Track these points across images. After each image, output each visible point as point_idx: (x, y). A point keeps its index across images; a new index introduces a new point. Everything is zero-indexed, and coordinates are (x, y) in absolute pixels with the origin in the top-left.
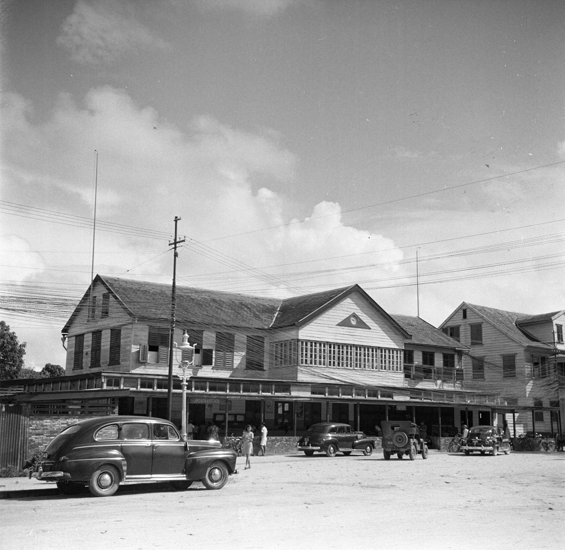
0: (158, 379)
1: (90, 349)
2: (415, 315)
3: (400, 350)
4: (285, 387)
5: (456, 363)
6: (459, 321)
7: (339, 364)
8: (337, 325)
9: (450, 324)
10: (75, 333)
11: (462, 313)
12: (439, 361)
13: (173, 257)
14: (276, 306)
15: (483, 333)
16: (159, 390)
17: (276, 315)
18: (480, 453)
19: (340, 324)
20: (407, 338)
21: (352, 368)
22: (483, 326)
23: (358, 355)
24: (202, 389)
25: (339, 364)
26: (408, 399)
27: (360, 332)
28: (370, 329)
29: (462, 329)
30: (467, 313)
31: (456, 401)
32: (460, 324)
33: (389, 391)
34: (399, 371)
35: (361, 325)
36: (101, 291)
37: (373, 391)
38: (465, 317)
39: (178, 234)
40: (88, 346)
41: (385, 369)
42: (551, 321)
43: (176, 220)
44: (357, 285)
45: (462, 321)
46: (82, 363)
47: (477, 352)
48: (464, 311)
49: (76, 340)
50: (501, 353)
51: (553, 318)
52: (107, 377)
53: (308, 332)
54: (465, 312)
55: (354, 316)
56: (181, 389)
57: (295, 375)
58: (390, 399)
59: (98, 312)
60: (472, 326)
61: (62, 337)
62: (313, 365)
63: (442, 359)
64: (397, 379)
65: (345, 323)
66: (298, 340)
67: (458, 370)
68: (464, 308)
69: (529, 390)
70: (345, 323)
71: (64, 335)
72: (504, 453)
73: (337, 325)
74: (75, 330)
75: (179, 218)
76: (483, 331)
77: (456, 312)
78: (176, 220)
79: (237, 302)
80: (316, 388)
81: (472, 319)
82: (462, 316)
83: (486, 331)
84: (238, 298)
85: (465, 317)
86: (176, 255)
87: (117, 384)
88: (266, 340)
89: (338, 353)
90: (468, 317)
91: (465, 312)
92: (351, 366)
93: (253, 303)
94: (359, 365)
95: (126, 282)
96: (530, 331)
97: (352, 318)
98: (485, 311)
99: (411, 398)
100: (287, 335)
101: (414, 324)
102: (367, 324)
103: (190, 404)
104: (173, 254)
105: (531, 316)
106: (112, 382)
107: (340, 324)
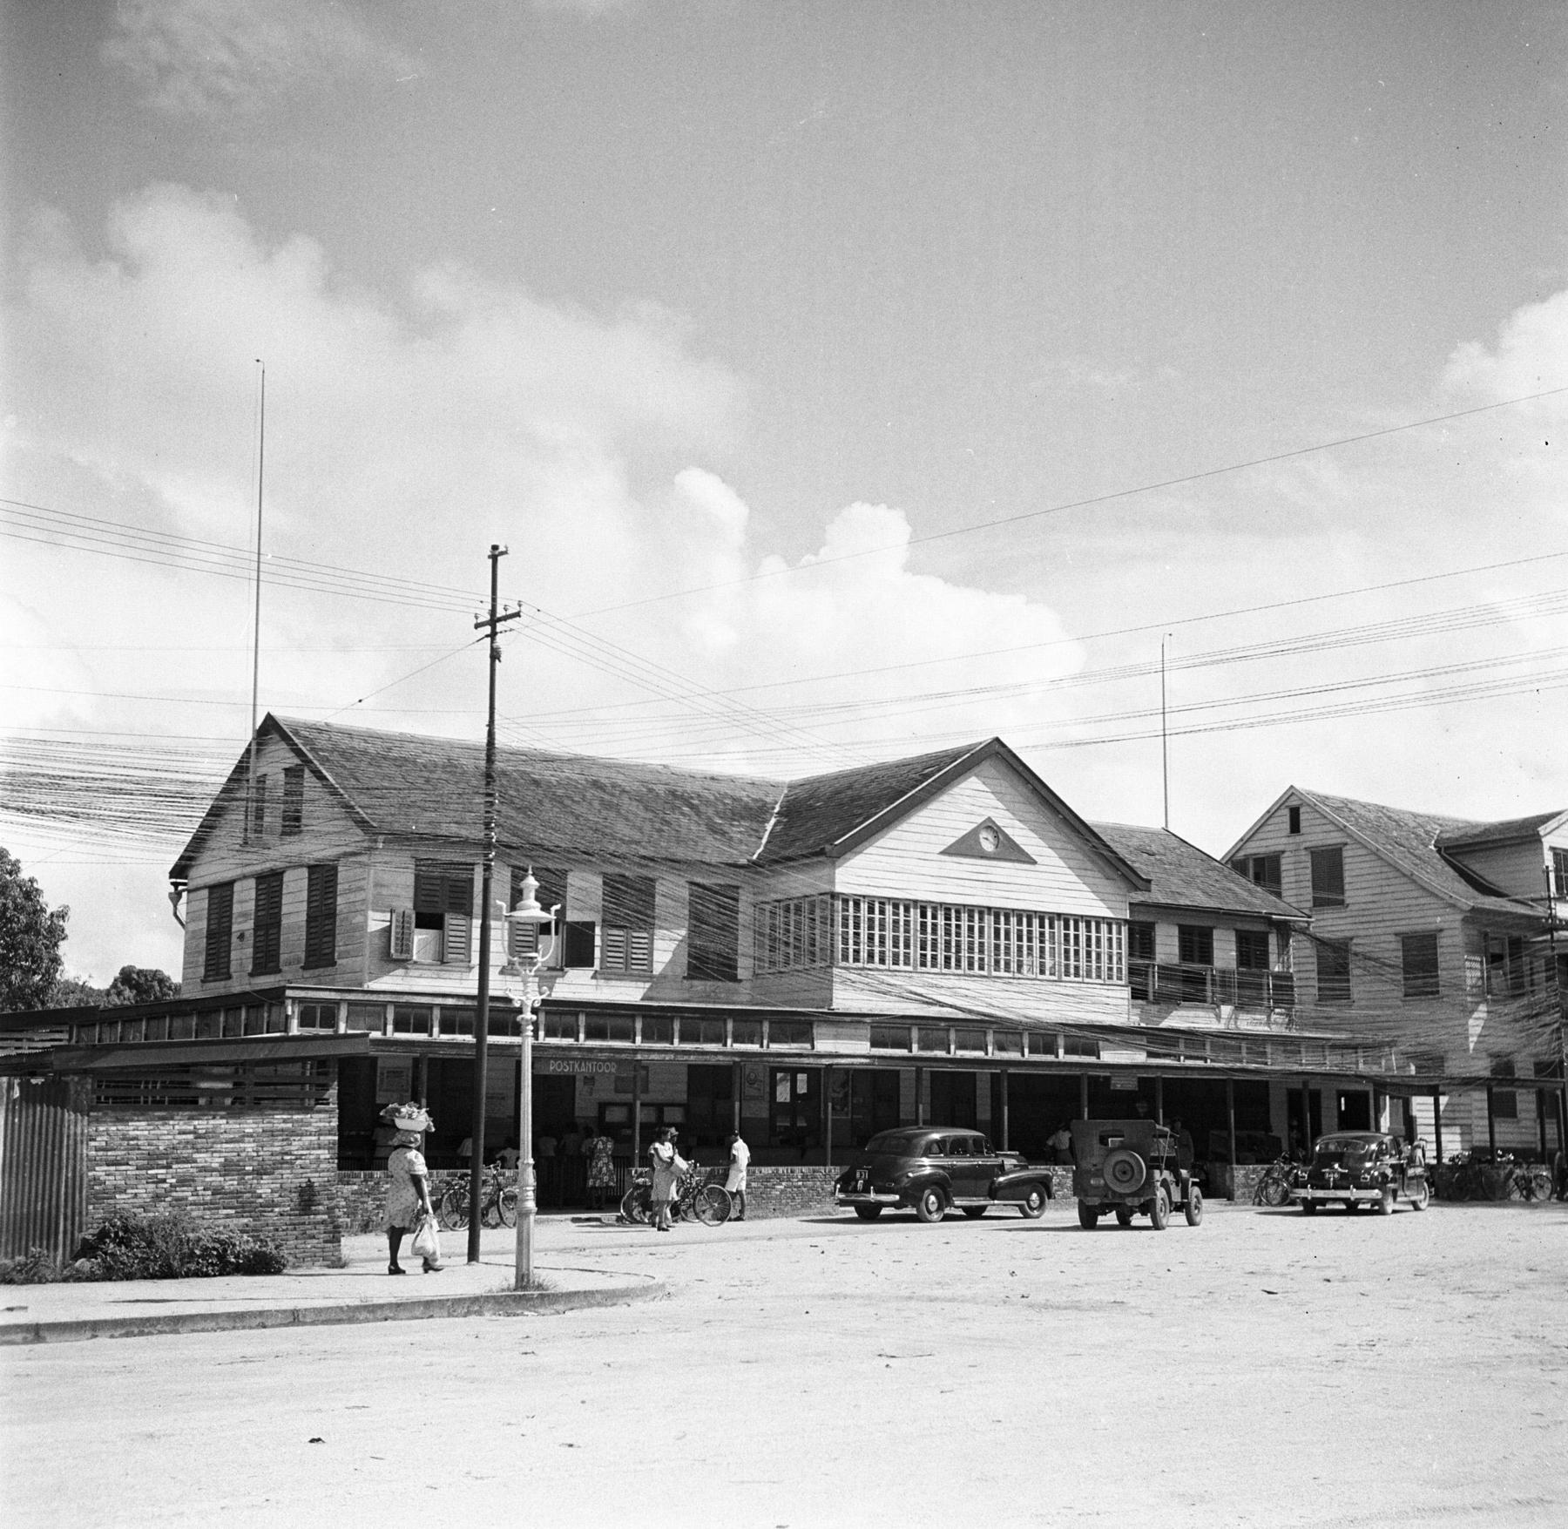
1: (250, 924)
2: (1157, 824)
3: (1119, 922)
4: (798, 1026)
5: (1273, 958)
6: (1277, 839)
9: (1256, 848)
11: (1287, 819)
12: (1225, 953)
14: (768, 800)
15: (1346, 874)
16: (445, 1037)
19: (953, 851)
20: (1137, 888)
21: (984, 973)
24: (565, 1035)
27: (1005, 870)
28: (1035, 863)
29: (1286, 864)
30: (1302, 817)
31: (1276, 1063)
33: (1088, 1036)
35: (1010, 851)
36: (276, 761)
38: (1295, 828)
40: (244, 915)
42: (1537, 840)
43: (495, 554)
44: (997, 739)
45: (1284, 840)
46: (229, 962)
47: (1330, 924)
50: (1399, 929)
51: (1542, 830)
52: (301, 1000)
53: (865, 872)
54: (1295, 813)
55: (990, 826)
57: (825, 993)
58: (1092, 1059)
59: (272, 819)
61: (172, 889)
62: (976, 971)
64: (1109, 1003)
65: (965, 848)
66: (834, 896)
67: (1277, 976)
68: (1294, 802)
69: (1475, 1031)
70: (965, 848)
71: (176, 885)
74: (209, 871)
75: (502, 549)
76: (1346, 867)
77: (1270, 815)
78: (495, 554)
79: (660, 789)
80: (886, 1029)
81: (1315, 834)
82: (1287, 826)
83: (1354, 867)
85: (1295, 828)
87: (330, 1019)
88: (745, 899)
89: (947, 931)
90: (1303, 830)
91: (1295, 813)
93: (706, 793)
94: (1004, 964)
96: (1476, 866)
97: (983, 834)
98: (1351, 810)
99: (873, 1045)
100: (798, 883)
102: (1026, 849)
104: (488, 652)
105: (1477, 826)
107: (953, 851)
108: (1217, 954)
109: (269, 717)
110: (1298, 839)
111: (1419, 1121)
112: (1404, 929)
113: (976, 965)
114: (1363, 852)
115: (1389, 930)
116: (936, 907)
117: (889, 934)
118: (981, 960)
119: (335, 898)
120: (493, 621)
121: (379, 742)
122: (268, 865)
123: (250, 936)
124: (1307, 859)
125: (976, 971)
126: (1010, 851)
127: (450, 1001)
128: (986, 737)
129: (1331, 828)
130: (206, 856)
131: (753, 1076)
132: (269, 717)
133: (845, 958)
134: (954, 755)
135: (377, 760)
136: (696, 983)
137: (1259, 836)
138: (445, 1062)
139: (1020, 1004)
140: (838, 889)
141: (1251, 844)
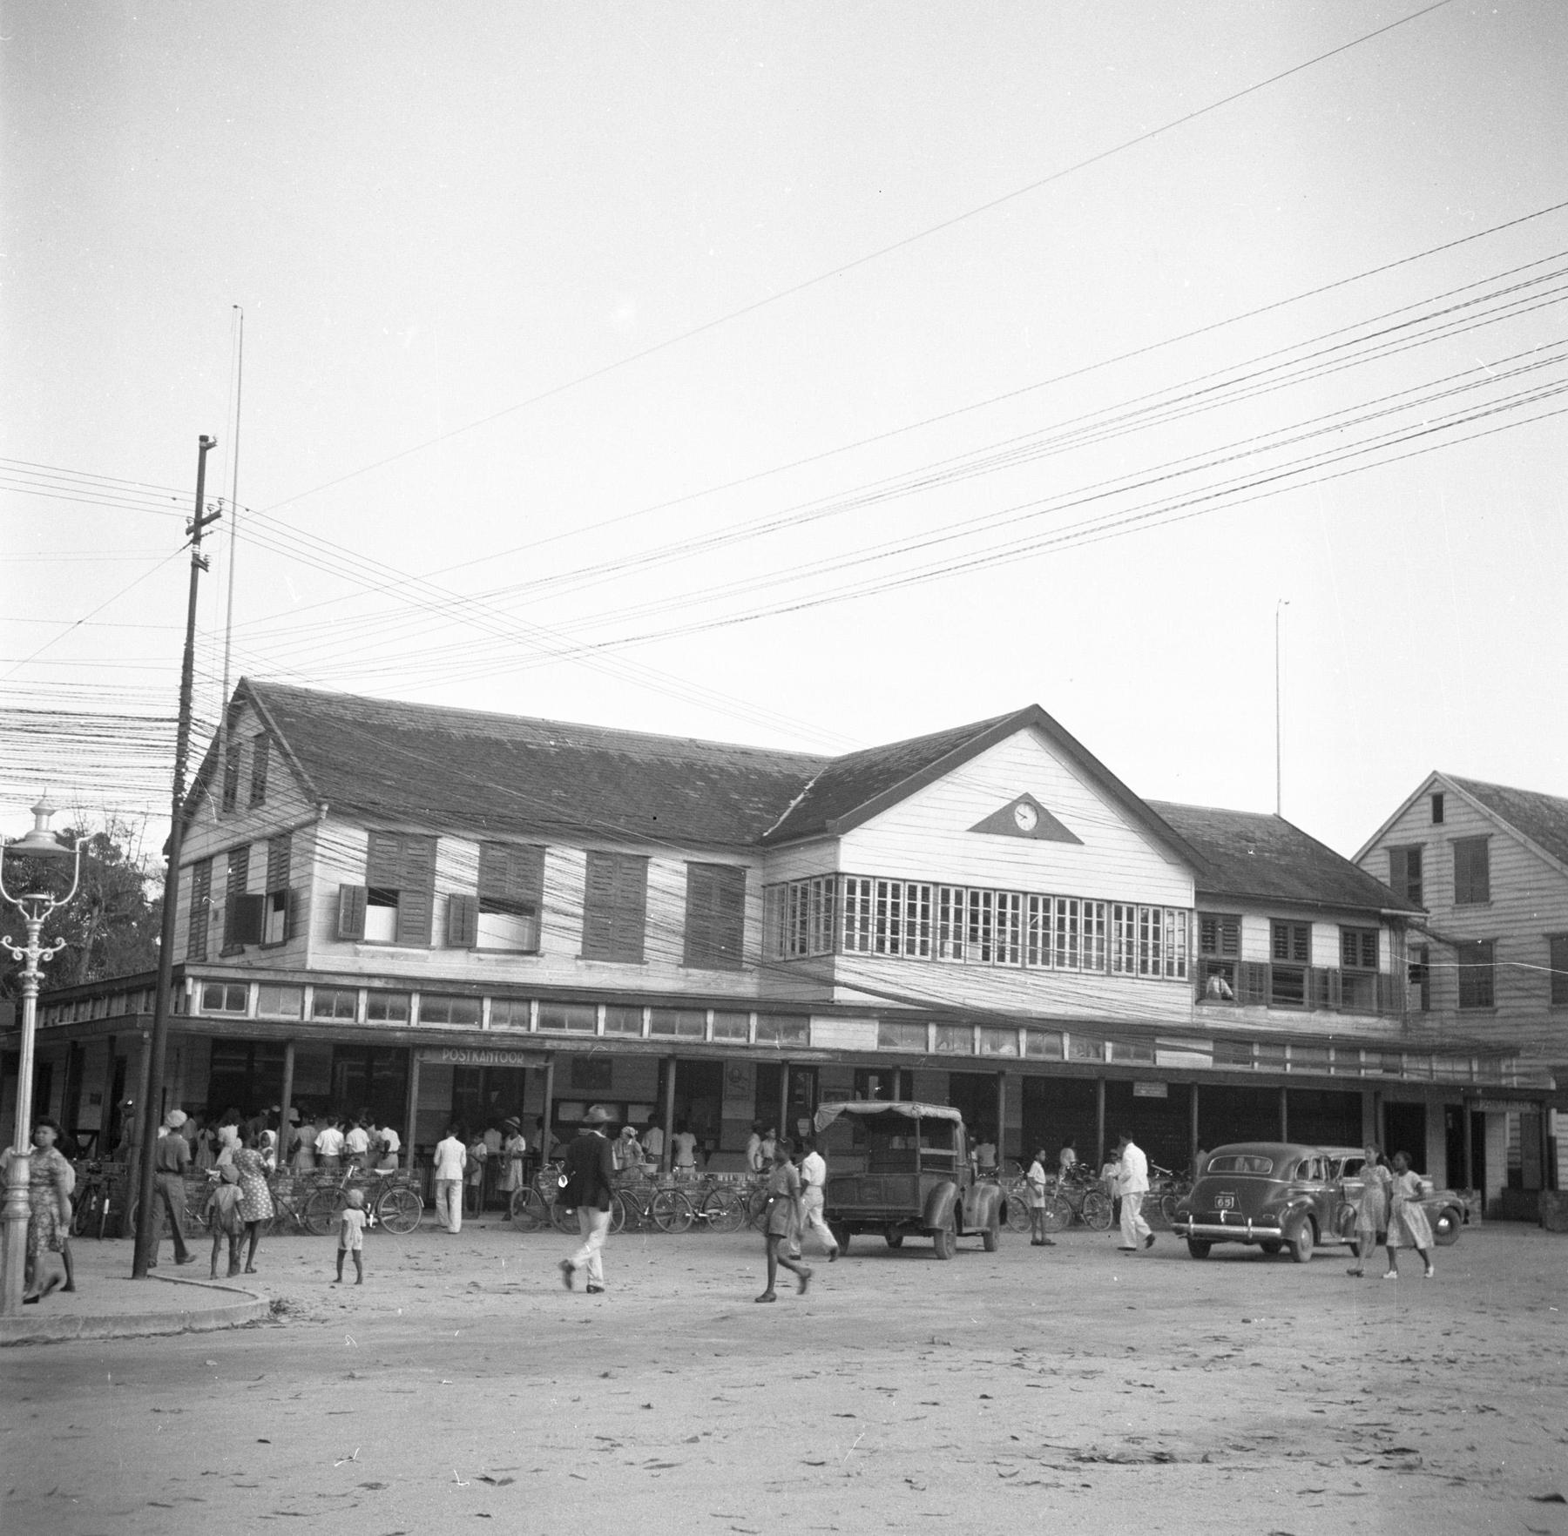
0: (370, 990)
1: (222, 902)
2: (1265, 808)
4: (798, 1015)
6: (1419, 830)
7: (881, 943)
8: (971, 830)
9: (1394, 839)
10: (193, 856)
13: (190, 568)
15: (1492, 868)
16: (372, 1022)
17: (793, 803)
18: (1257, 1248)
21: (1019, 965)
22: (1491, 845)
23: (981, 918)
24: (340, 1014)
25: (881, 943)
26: (1206, 1062)
27: (1047, 850)
28: (1081, 843)
29: (1428, 857)
30: (1446, 805)
31: (1369, 1068)
32: (1420, 840)
33: (1144, 1034)
34: (1150, 975)
35: (1051, 829)
36: (250, 727)
37: (1092, 1030)
38: (1438, 817)
39: (206, 491)
40: (218, 891)
41: (1073, 964)
43: (205, 444)
45: (1426, 831)
46: (205, 943)
47: (1473, 924)
48: (1436, 798)
49: (195, 876)
50: (1546, 930)
52: (204, 979)
53: (872, 849)
54: (1438, 801)
56: (350, 1015)
58: (1146, 1063)
59: (243, 792)
60: (1460, 845)
62: (1008, 963)
63: (1267, 936)
64: (1170, 1001)
65: (999, 824)
66: (838, 874)
68: (1436, 790)
70: (999, 824)
72: (1347, 1250)
73: (971, 830)
75: (211, 440)
76: (1492, 860)
77: (1412, 802)
78: (205, 444)
81: (1461, 822)
82: (1429, 815)
84: (685, 753)
85: (1438, 817)
86: (198, 564)
87: (239, 1002)
88: (753, 879)
90: (1447, 819)
91: (1438, 801)
92: (1014, 959)
94: (1038, 953)
95: (328, 700)
97: (1022, 809)
98: (1502, 798)
99: (1217, 1059)
100: (802, 864)
101: (1258, 834)
103: (995, 1079)
104: (190, 559)
106: (221, 998)
108: (680, 883)
109: (243, 683)
110: (1443, 829)
111: (1559, 1142)
112: (1553, 929)
113: (1008, 957)
114: (1509, 843)
115: (1534, 931)
116: (1102, 903)
117: (903, 916)
118: (924, 943)
119: (287, 873)
120: (201, 521)
121: (360, 709)
122: (236, 840)
123: (222, 913)
124: (1449, 850)
125: (1008, 963)
126: (1051, 829)
127: (377, 984)
128: (1022, 704)
129: (1477, 817)
130: (195, 831)
131: (736, 1073)
132: (243, 683)
133: (850, 945)
134: (987, 725)
135: (409, 738)
136: (691, 971)
137: (1400, 826)
138: (690, 1062)
139: (961, 992)
140: (843, 868)
141: (1391, 835)
